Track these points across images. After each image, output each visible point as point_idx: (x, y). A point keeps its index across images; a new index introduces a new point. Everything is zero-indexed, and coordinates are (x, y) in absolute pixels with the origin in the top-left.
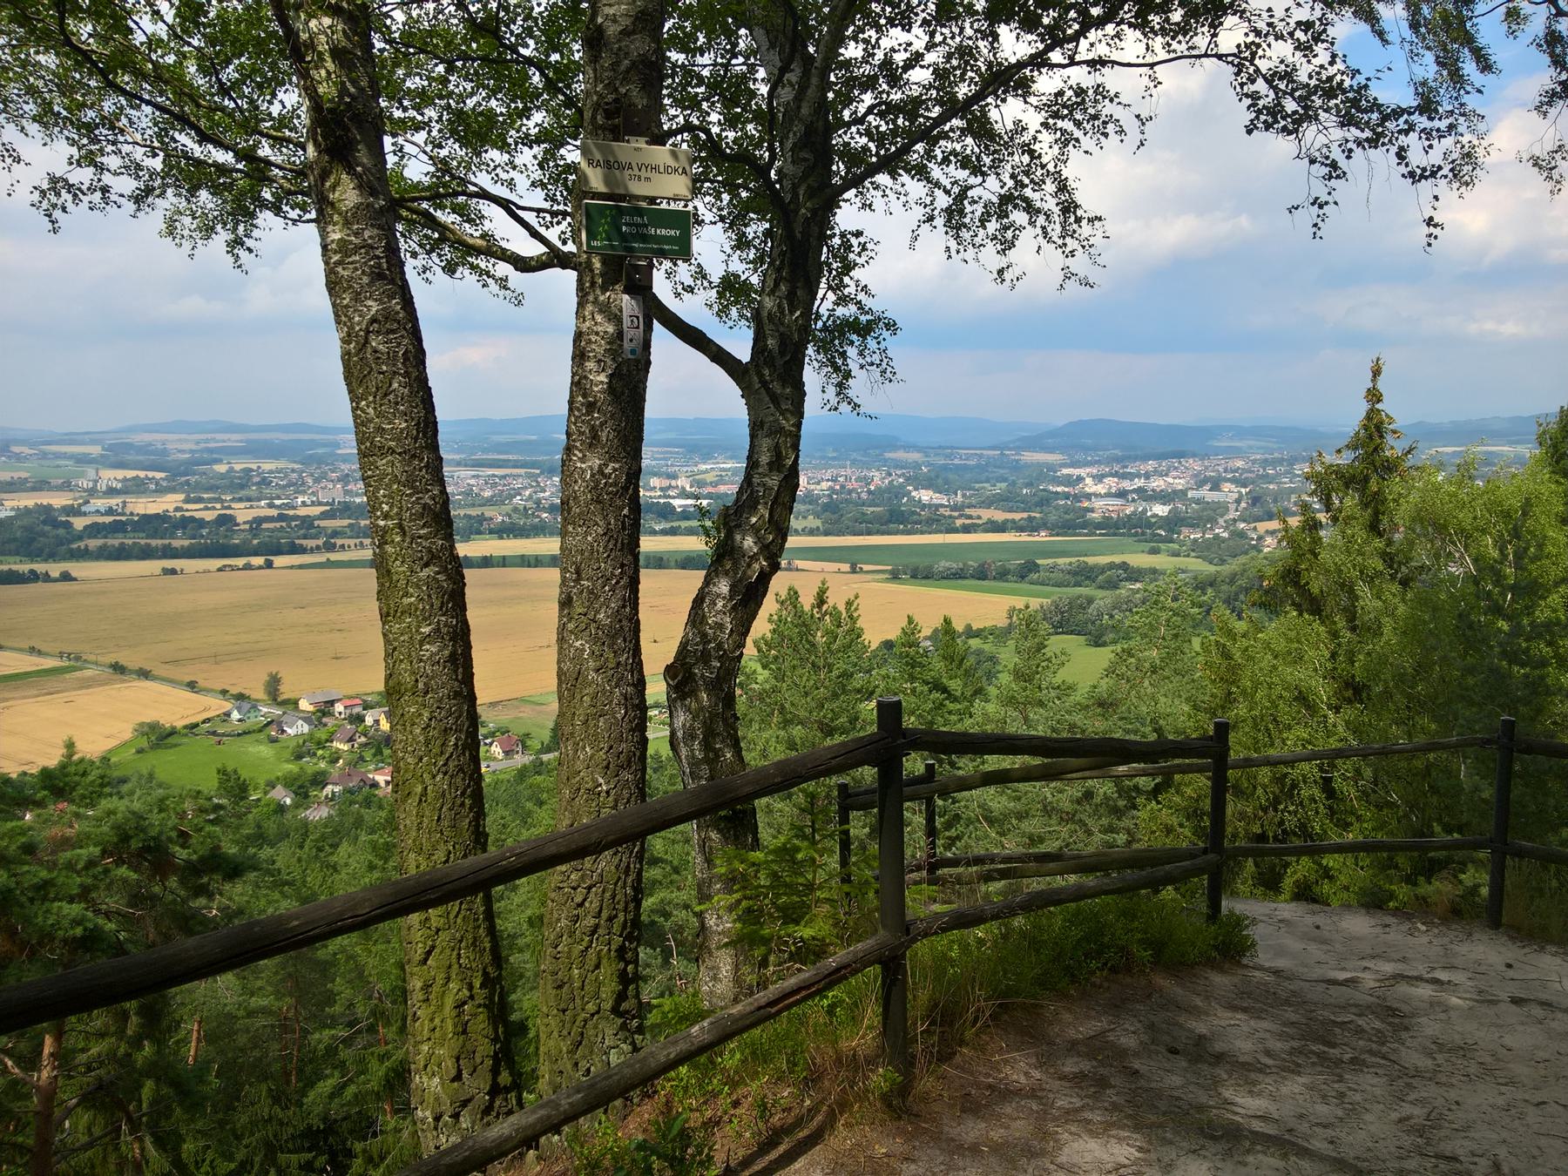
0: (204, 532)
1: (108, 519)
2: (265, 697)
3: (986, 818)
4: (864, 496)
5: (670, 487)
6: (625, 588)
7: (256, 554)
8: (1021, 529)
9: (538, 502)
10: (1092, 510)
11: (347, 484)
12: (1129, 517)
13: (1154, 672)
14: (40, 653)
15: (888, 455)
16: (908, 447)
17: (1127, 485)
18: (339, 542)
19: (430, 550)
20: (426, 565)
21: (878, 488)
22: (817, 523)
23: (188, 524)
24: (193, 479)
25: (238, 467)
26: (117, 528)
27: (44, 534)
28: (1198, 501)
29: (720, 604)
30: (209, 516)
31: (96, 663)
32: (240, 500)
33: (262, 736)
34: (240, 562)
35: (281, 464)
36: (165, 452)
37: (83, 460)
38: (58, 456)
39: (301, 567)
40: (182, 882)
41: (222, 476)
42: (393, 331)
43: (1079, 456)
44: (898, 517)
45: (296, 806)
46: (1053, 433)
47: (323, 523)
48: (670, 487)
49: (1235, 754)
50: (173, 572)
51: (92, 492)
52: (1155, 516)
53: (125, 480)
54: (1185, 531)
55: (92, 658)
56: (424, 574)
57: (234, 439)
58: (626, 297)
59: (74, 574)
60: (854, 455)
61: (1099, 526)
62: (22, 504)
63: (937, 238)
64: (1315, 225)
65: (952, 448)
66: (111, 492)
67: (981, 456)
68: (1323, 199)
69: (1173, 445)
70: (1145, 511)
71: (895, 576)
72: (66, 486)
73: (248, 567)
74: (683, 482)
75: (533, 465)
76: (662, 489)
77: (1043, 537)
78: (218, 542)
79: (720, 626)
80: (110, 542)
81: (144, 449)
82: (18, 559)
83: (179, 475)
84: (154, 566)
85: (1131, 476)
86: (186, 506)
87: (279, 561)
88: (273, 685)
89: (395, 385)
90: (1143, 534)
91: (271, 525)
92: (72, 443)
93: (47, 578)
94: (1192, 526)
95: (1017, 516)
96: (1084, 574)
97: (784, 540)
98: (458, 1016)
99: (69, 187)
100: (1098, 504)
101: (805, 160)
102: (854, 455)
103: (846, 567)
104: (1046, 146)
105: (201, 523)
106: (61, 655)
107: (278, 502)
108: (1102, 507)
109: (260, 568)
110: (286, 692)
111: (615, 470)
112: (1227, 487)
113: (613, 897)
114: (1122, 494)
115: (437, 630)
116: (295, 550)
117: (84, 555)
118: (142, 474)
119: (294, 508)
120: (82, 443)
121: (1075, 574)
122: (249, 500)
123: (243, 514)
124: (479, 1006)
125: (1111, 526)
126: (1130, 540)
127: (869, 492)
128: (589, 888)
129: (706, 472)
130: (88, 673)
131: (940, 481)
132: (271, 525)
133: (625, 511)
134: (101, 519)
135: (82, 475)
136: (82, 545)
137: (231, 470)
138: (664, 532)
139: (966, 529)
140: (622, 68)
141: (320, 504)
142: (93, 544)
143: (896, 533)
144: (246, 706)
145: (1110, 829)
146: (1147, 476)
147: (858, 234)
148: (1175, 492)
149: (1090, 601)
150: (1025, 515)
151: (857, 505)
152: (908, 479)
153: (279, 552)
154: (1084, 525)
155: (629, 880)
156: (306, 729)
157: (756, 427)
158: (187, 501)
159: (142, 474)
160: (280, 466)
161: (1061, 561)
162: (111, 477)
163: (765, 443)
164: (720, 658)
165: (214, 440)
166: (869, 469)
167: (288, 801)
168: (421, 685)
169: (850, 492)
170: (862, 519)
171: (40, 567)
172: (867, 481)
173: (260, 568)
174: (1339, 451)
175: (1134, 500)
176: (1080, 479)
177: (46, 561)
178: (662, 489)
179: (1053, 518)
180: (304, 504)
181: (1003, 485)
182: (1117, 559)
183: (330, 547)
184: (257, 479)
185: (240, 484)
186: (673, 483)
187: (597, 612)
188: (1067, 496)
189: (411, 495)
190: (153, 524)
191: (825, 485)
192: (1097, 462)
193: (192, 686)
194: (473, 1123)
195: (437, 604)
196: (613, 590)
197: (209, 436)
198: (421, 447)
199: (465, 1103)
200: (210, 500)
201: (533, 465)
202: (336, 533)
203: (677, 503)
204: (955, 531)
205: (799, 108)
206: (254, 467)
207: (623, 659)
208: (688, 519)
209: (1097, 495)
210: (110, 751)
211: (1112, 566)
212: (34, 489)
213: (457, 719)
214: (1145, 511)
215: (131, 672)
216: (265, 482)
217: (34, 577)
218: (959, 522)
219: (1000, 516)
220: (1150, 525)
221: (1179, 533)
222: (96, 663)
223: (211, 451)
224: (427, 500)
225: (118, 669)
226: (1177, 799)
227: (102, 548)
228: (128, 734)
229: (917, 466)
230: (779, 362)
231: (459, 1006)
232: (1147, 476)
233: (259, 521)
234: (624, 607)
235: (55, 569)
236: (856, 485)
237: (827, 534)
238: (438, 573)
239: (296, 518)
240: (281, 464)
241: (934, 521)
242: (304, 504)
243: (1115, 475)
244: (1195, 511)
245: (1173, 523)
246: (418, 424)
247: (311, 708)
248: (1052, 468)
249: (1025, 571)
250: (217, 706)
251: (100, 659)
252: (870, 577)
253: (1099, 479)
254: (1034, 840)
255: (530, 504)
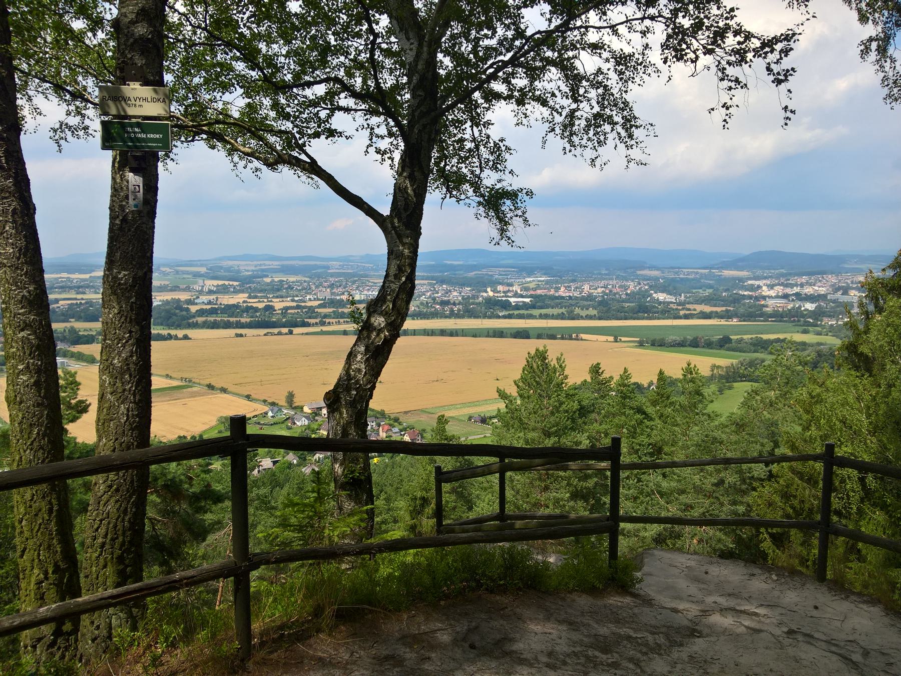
0: (258, 314)
1: (209, 307)
2: (286, 404)
3: (659, 492)
4: (624, 297)
5: (509, 291)
6: (133, 345)
7: (284, 327)
8: (721, 317)
9: (434, 299)
10: (767, 306)
11: (333, 289)
12: (789, 310)
13: (771, 405)
14: (171, 377)
15: (639, 272)
16: (651, 268)
17: (789, 291)
18: (327, 320)
19: (25, 322)
20: (22, 330)
21: (633, 292)
22: (595, 312)
23: (249, 309)
24: (253, 286)
25: (276, 279)
26: (213, 312)
27: (175, 315)
28: (834, 301)
29: (359, 357)
30: (261, 306)
31: (199, 384)
32: (277, 297)
33: (283, 426)
34: (276, 331)
35: (299, 278)
36: (239, 271)
37: (197, 275)
38: (184, 273)
39: (307, 334)
40: (190, 505)
41: (268, 284)
42: (6, 198)
43: (759, 272)
44: (644, 309)
45: (299, 465)
46: (743, 259)
47: (319, 310)
48: (509, 291)
49: (625, 459)
50: (241, 336)
51: (201, 292)
52: (806, 310)
53: (218, 286)
54: (825, 320)
55: (197, 381)
56: (20, 335)
57: (275, 264)
58: (131, 174)
59: (190, 336)
60: (619, 273)
61: (771, 316)
62: (165, 298)
63: (557, 142)
64: (725, 120)
65: (679, 268)
66: (211, 292)
67: (697, 273)
68: (728, 104)
69: (817, 267)
70: (800, 307)
71: (641, 344)
72: (188, 289)
73: (280, 334)
74: (516, 288)
75: (432, 278)
76: (504, 292)
77: (735, 322)
78: (265, 321)
79: (359, 370)
80: (209, 319)
81: (228, 269)
82: (162, 327)
83: (247, 283)
84: (232, 332)
85: (792, 286)
86: (249, 300)
87: (296, 330)
88: (290, 397)
89: (7, 228)
90: (799, 321)
91: (292, 311)
92: (191, 266)
93: (176, 338)
94: (830, 316)
95: (719, 309)
96: (761, 345)
97: (403, 320)
98: (38, 588)
99: (70, 128)
100: (770, 302)
101: (420, 96)
102: (619, 273)
103: (611, 339)
104: (613, 80)
105: (256, 310)
106: (182, 379)
107: (296, 299)
108: (772, 305)
109: (286, 334)
110: (297, 402)
111: (125, 275)
112: (853, 293)
113: (115, 526)
114: (786, 296)
115: (28, 367)
116: (305, 324)
117: (195, 326)
118: (227, 283)
119: (305, 302)
120: (196, 266)
121: (754, 345)
122: (282, 297)
123: (278, 305)
124: (51, 584)
125: (779, 316)
126: (791, 324)
127: (627, 294)
128: (101, 521)
129: (530, 282)
130: (195, 389)
131: (671, 288)
132: (292, 311)
133: (132, 300)
134: (205, 307)
135: (195, 283)
136: (195, 320)
137: (273, 281)
138: (505, 317)
139: (686, 317)
140: (129, 43)
141: (318, 300)
142: (200, 320)
143: (643, 318)
144: (276, 409)
145: (734, 503)
146: (802, 285)
147: (502, 140)
148: (819, 296)
149: (763, 361)
150: (724, 309)
151: (618, 301)
152: (651, 287)
153: (296, 326)
154: (762, 315)
155: (127, 518)
156: (307, 422)
157: (390, 253)
158: (249, 297)
159: (227, 283)
160: (299, 279)
161: (745, 337)
162: (211, 284)
163: (395, 263)
164: (356, 389)
165: (265, 265)
166: (627, 281)
167: (295, 462)
168: (18, 399)
169: (615, 294)
170: (621, 310)
171: (173, 332)
172: (626, 288)
173: (286, 334)
174: (884, 270)
175: (793, 300)
176: (759, 287)
177: (176, 329)
178: (504, 292)
179: (742, 310)
180: (310, 299)
181: (711, 291)
182: (781, 336)
183: (323, 324)
184: (286, 286)
185: (277, 289)
186: (511, 289)
187: (114, 358)
188: (750, 297)
189: (15, 290)
190: (231, 309)
191: (600, 290)
192: (770, 277)
193: (248, 397)
194: (42, 652)
195: (28, 352)
196: (124, 346)
197: (259, 263)
198: (22, 263)
199: (39, 640)
200: (262, 297)
201: (432, 278)
202: (326, 316)
203: (512, 300)
204: (680, 318)
205: (417, 65)
206: (285, 279)
207: (127, 387)
208: (518, 309)
209: (770, 297)
210: (205, 431)
211: (778, 340)
212: (171, 290)
213: (39, 419)
214: (800, 307)
215: (217, 389)
216: (290, 288)
217: (170, 337)
218: (682, 313)
219: (707, 309)
220: (803, 316)
221: (821, 321)
222: (199, 384)
223: (263, 270)
224: (25, 293)
225: (210, 387)
226: (776, 485)
227: (205, 322)
228: (214, 423)
229: (656, 279)
230: (404, 215)
231: (39, 583)
232: (802, 285)
233: (287, 308)
234: (131, 356)
235: (180, 333)
236: (618, 290)
237: (600, 319)
238: (29, 335)
239: (305, 307)
240: (299, 278)
241: (666, 312)
242: (310, 299)
243: (782, 284)
244: (832, 308)
245: (818, 314)
246: (20, 250)
247: (310, 411)
248: (741, 280)
249: (724, 344)
250: (262, 408)
251: (202, 382)
252: (626, 344)
253: (771, 287)
254: (689, 507)
255: (430, 300)
